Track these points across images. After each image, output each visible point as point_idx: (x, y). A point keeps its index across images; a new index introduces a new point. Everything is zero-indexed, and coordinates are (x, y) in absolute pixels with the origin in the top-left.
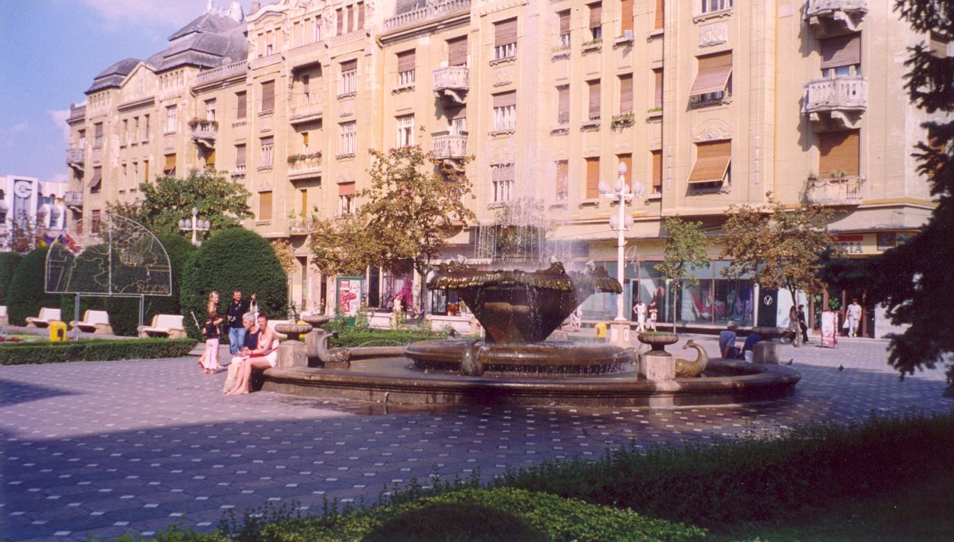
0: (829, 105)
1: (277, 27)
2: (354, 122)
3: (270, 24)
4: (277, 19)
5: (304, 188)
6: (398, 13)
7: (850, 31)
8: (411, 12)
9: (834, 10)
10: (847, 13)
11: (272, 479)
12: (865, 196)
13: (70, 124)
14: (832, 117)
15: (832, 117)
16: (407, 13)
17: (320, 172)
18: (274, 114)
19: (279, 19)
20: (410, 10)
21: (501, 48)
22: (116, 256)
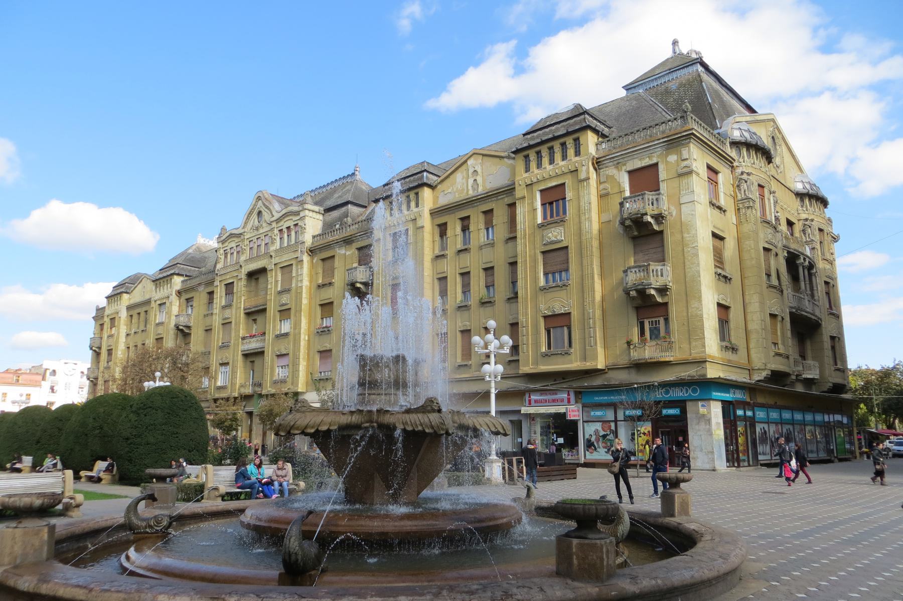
1: (296, 223)
3: (289, 221)
4: (237, 240)
5: (252, 360)
22: (804, 295)
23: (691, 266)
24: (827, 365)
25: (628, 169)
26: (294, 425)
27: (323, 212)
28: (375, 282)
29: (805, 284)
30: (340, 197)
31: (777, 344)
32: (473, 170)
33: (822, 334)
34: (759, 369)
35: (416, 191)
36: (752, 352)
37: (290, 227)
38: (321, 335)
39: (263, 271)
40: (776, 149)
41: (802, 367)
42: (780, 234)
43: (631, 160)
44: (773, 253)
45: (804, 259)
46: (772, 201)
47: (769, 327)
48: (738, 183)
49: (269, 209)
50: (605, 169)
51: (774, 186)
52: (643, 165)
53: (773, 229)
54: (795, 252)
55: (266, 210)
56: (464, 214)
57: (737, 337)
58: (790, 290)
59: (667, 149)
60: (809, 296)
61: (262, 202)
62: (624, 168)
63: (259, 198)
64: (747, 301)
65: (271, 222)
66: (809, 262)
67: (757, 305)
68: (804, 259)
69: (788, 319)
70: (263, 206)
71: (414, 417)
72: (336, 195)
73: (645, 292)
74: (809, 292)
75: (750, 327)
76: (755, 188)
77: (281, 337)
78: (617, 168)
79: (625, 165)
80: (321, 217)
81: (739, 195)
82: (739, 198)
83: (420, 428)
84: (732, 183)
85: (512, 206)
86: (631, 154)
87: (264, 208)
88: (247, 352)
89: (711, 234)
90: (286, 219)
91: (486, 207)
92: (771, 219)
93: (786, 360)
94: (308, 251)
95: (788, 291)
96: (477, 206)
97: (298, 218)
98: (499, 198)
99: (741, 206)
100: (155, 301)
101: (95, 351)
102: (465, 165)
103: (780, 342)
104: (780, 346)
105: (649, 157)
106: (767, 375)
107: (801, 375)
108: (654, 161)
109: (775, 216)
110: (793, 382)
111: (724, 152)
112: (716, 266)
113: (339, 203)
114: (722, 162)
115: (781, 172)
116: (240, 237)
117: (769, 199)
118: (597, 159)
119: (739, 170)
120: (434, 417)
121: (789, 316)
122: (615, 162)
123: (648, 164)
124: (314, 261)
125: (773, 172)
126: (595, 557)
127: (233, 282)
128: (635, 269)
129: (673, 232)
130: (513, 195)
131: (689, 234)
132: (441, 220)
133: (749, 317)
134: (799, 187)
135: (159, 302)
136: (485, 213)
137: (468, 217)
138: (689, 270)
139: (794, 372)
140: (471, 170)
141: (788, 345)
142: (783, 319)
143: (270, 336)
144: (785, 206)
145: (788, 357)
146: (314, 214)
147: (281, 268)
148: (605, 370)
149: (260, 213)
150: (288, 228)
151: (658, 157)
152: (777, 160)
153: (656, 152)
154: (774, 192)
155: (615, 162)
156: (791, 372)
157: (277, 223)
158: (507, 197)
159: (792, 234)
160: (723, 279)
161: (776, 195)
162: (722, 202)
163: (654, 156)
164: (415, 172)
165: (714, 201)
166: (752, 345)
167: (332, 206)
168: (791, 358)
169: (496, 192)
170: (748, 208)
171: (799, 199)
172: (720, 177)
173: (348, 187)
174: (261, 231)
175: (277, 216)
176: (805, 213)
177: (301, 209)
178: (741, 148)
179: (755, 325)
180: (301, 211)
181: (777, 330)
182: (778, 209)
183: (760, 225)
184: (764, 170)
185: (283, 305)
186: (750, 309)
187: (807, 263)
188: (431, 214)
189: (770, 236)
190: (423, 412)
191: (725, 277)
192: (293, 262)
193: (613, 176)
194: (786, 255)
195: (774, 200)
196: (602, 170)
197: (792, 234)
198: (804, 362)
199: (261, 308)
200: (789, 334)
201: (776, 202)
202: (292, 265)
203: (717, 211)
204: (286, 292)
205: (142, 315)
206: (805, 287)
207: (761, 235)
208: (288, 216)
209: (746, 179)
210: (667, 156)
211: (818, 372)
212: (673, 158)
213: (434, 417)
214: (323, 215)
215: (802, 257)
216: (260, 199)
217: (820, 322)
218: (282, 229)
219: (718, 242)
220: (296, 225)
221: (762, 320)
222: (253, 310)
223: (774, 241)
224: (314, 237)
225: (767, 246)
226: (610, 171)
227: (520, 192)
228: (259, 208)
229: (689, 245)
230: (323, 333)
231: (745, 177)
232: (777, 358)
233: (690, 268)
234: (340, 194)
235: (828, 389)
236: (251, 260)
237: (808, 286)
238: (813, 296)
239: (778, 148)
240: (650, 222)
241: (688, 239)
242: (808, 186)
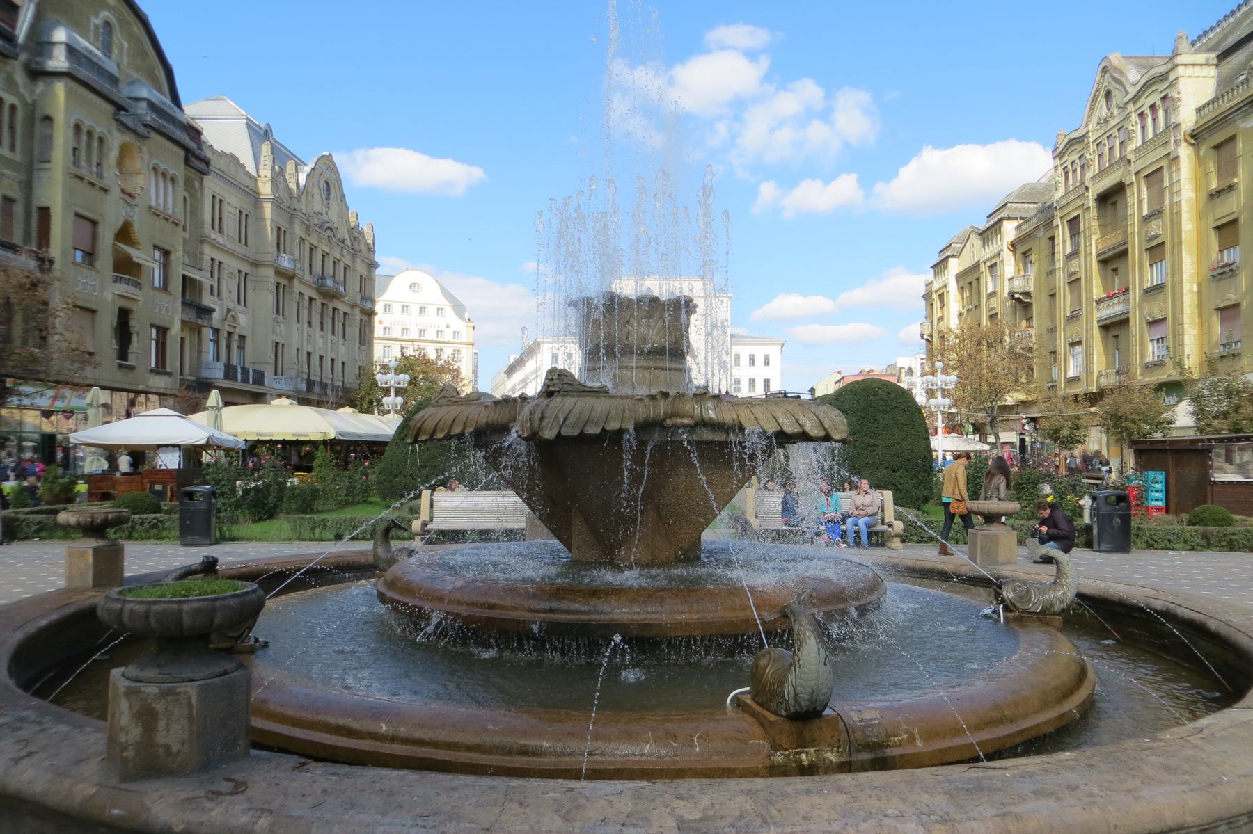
1: (1163, 94)
38: (1220, 280)
55: (1117, 86)
100: (985, 263)
101: (1018, 300)
135: (989, 264)
146: (1197, 69)
147: (1147, 176)
150: (1153, 107)
157: (1134, 103)
192: (1080, 212)
204: (1156, 216)
205: (974, 284)
230: (1223, 276)
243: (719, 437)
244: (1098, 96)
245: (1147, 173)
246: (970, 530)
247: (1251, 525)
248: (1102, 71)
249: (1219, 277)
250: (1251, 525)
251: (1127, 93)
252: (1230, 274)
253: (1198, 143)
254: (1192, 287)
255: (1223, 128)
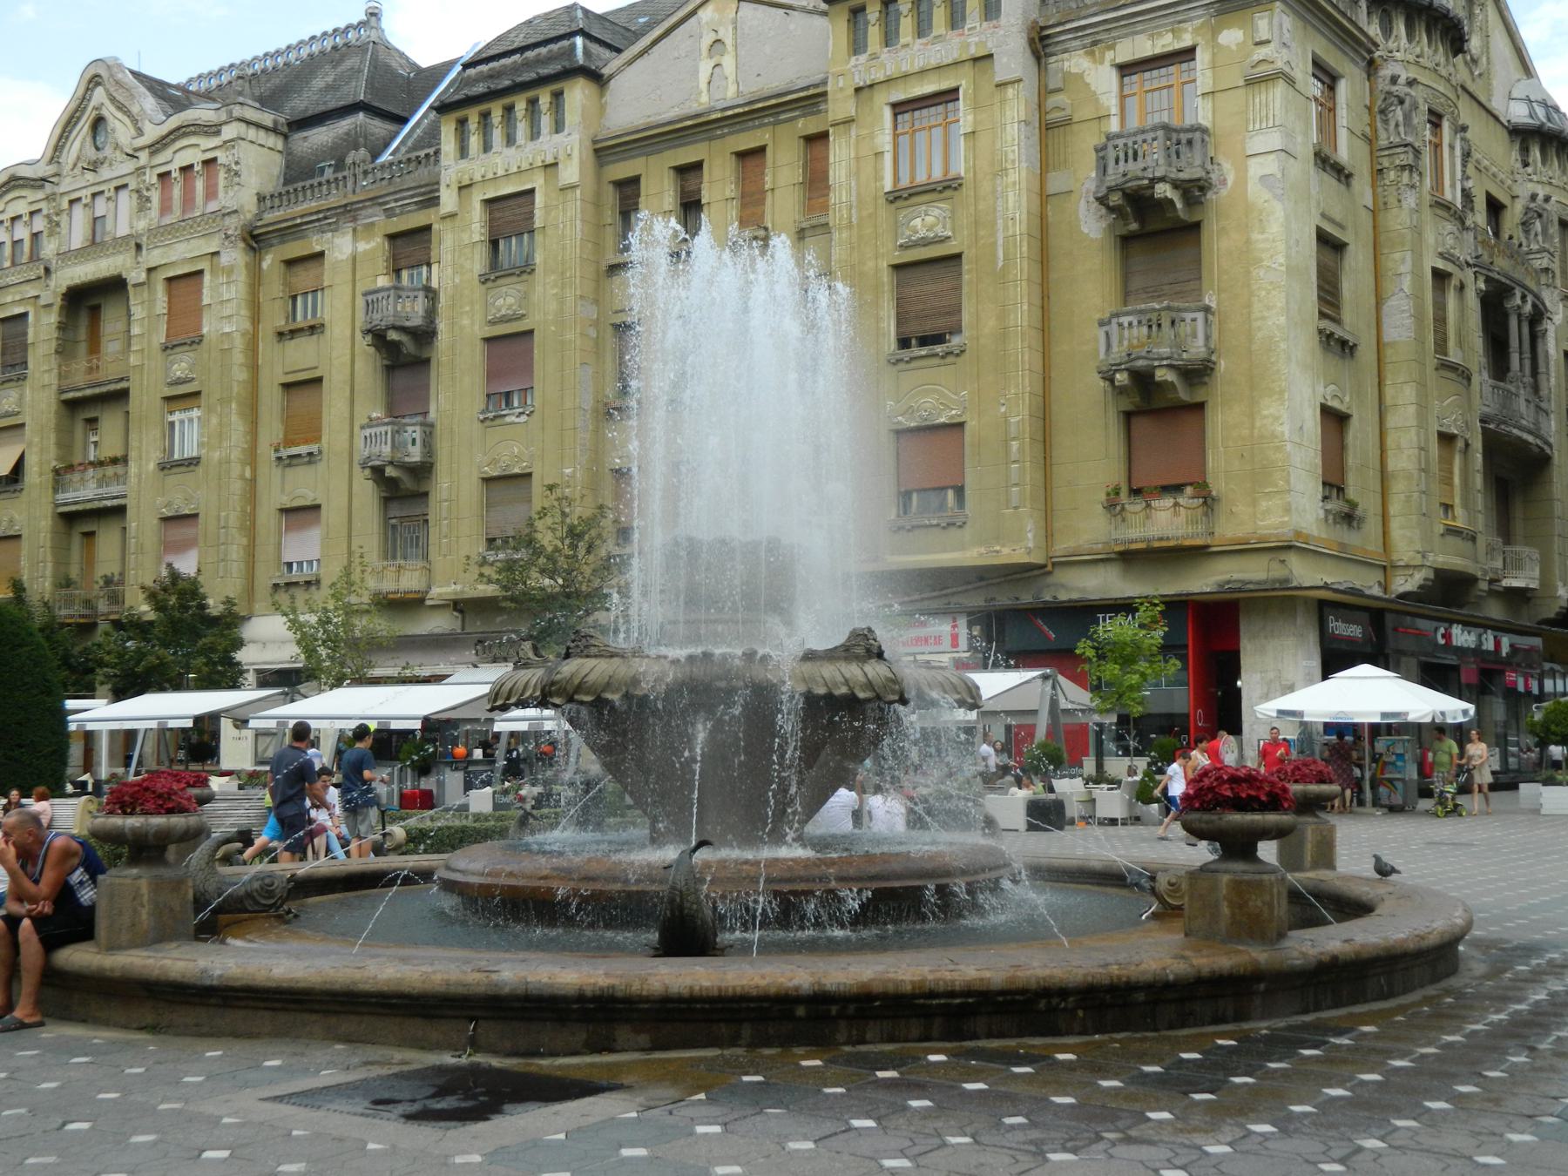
0: (1151, 355)
1: (209, 155)
2: (197, 394)
3: (190, 151)
4: (32, 195)
5: (87, 529)
6: (285, 184)
7: (1183, 221)
8: (315, 182)
9: (1154, 181)
10: (1176, 185)
11: (222, 1118)
12: (1228, 529)
13: (557, 132)
14: (1157, 379)
15: (1157, 379)
16: (308, 183)
17: (124, 497)
18: (28, 383)
19: (40, 195)
20: (312, 177)
21: (299, 299)
22: (1518, 388)
23: (1266, 314)
24: (1556, 557)
25: (1118, 60)
26: (580, 683)
27: (285, 129)
28: (442, 326)
29: (1521, 359)
30: (330, 88)
31: (1452, 506)
32: (713, 37)
33: (1551, 481)
34: (1407, 566)
35: (555, 87)
36: (1395, 525)
37: (191, 166)
38: (289, 465)
39: (115, 286)
40: (1471, 15)
41: (1501, 559)
42: (1471, 234)
43: (1126, 36)
44: (1454, 282)
45: (1524, 297)
46: (1458, 152)
47: (1435, 467)
48: (1380, 108)
49: (128, 113)
50: (1060, 57)
51: (1466, 113)
52: (1158, 51)
53: (1457, 223)
54: (1503, 280)
55: (119, 115)
56: (686, 155)
57: (1360, 487)
58: (1485, 375)
59: (1220, 13)
60: (1528, 389)
61: (107, 91)
62: (1109, 55)
63: (94, 81)
64: (1388, 400)
65: (136, 150)
66: (1534, 306)
67: (1412, 409)
68: (1524, 297)
69: (1477, 444)
70: (107, 103)
71: (829, 671)
72: (318, 83)
73: (1153, 376)
74: (1528, 379)
75: (1393, 464)
76: (1420, 118)
77: (175, 470)
78: (1092, 54)
79: (1112, 47)
80: (275, 142)
81: (1382, 135)
82: (1383, 143)
83: (844, 690)
84: (1368, 103)
85: (818, 140)
86: (1129, 24)
87: (112, 109)
88: (73, 508)
89: (1314, 236)
90: (179, 144)
91: (746, 141)
92: (1454, 196)
93: (1470, 543)
94: (249, 238)
95: (1481, 378)
96: (723, 136)
97: (215, 141)
98: (782, 117)
99: (1386, 163)
102: (693, 20)
103: (1457, 501)
104: (1459, 511)
105: (1173, 31)
106: (1425, 579)
107: (1498, 581)
108: (1186, 41)
109: (1463, 190)
110: (1481, 597)
111: (1350, 20)
112: (1322, 315)
113: (332, 105)
114: (1347, 49)
115: (1480, 75)
116: (42, 187)
117: (1452, 147)
118: (1043, 28)
119: (1386, 72)
120: (875, 670)
121: (1480, 436)
122: (1088, 41)
123: (1170, 48)
124: (265, 265)
125: (1462, 75)
126: (1259, 903)
127: (24, 315)
128: (1130, 318)
129: (1223, 228)
130: (819, 112)
131: (1263, 233)
132: (623, 170)
133: (1390, 441)
134: (1518, 113)
136: (742, 156)
137: (697, 166)
138: (1259, 323)
139: (1485, 572)
140: (708, 39)
141: (1471, 513)
142: (1467, 445)
143: (144, 463)
144: (1486, 163)
145: (1473, 539)
146: (262, 133)
147: (170, 280)
148: (1044, 566)
149: (98, 123)
150: (187, 169)
151: (1196, 31)
152: (1474, 44)
153: (1190, 19)
154: (1464, 129)
155: (1088, 41)
156: (1479, 574)
157: (152, 154)
158: (804, 115)
159: (1497, 234)
160: (1338, 348)
161: (1468, 135)
162: (1345, 150)
163: (1186, 30)
164: (553, 34)
165: (1327, 150)
166: (1395, 508)
167: (310, 113)
168: (1482, 541)
169: (773, 102)
170: (1403, 168)
171: (1517, 146)
172: (1343, 87)
173: (352, 62)
174: (105, 173)
175: (152, 133)
176: (1531, 180)
177: (224, 117)
178: (1394, 14)
179: (1403, 460)
180: (226, 123)
181: (1451, 472)
182: (1471, 170)
183: (1427, 214)
184: (1444, 72)
185: (179, 382)
186: (1392, 421)
187: (1528, 308)
188: (596, 151)
189: (1450, 241)
190: (846, 659)
191: (1343, 343)
192: (203, 265)
193: (1080, 76)
194: (1482, 286)
195: (1462, 148)
196: (1052, 59)
197: (1497, 234)
198: (1508, 548)
199: (112, 387)
200: (1478, 481)
201: (1467, 155)
202: (200, 272)
203: (1330, 180)
204: (186, 348)
206: (1521, 365)
207: (1430, 238)
208: (185, 135)
209: (1402, 95)
210: (1215, 32)
211: (1537, 573)
212: (1231, 37)
213: (875, 670)
214: (286, 137)
215: (1518, 293)
216: (98, 84)
217: (1548, 451)
218: (168, 173)
219: (1329, 257)
220: (207, 163)
221: (1422, 449)
222: (89, 392)
223: (1457, 253)
224: (261, 199)
225: (1440, 264)
226: (1073, 61)
227: (840, 105)
228: (96, 108)
229: (1261, 260)
230: (295, 461)
231: (1401, 89)
232: (1451, 540)
233: (1263, 318)
234: (330, 79)
235: (1557, 614)
236: (82, 254)
237: (1527, 363)
238: (1536, 388)
239: (1477, 11)
240: (1171, 202)
241: (1262, 246)
242: (1540, 112)
243: (944, 592)
244: (79, 119)
245: (171, 274)
246: (100, 877)
247: (1555, 969)
248: (90, 81)
249: (287, 462)
250: (1555, 969)
251: (140, 132)
252: (307, 459)
253: (260, 249)
254: (244, 471)
255: (696, 142)
